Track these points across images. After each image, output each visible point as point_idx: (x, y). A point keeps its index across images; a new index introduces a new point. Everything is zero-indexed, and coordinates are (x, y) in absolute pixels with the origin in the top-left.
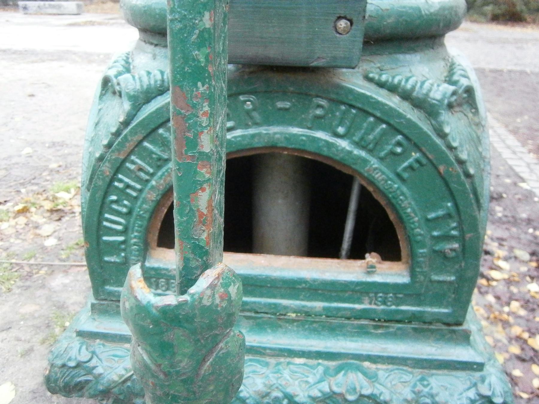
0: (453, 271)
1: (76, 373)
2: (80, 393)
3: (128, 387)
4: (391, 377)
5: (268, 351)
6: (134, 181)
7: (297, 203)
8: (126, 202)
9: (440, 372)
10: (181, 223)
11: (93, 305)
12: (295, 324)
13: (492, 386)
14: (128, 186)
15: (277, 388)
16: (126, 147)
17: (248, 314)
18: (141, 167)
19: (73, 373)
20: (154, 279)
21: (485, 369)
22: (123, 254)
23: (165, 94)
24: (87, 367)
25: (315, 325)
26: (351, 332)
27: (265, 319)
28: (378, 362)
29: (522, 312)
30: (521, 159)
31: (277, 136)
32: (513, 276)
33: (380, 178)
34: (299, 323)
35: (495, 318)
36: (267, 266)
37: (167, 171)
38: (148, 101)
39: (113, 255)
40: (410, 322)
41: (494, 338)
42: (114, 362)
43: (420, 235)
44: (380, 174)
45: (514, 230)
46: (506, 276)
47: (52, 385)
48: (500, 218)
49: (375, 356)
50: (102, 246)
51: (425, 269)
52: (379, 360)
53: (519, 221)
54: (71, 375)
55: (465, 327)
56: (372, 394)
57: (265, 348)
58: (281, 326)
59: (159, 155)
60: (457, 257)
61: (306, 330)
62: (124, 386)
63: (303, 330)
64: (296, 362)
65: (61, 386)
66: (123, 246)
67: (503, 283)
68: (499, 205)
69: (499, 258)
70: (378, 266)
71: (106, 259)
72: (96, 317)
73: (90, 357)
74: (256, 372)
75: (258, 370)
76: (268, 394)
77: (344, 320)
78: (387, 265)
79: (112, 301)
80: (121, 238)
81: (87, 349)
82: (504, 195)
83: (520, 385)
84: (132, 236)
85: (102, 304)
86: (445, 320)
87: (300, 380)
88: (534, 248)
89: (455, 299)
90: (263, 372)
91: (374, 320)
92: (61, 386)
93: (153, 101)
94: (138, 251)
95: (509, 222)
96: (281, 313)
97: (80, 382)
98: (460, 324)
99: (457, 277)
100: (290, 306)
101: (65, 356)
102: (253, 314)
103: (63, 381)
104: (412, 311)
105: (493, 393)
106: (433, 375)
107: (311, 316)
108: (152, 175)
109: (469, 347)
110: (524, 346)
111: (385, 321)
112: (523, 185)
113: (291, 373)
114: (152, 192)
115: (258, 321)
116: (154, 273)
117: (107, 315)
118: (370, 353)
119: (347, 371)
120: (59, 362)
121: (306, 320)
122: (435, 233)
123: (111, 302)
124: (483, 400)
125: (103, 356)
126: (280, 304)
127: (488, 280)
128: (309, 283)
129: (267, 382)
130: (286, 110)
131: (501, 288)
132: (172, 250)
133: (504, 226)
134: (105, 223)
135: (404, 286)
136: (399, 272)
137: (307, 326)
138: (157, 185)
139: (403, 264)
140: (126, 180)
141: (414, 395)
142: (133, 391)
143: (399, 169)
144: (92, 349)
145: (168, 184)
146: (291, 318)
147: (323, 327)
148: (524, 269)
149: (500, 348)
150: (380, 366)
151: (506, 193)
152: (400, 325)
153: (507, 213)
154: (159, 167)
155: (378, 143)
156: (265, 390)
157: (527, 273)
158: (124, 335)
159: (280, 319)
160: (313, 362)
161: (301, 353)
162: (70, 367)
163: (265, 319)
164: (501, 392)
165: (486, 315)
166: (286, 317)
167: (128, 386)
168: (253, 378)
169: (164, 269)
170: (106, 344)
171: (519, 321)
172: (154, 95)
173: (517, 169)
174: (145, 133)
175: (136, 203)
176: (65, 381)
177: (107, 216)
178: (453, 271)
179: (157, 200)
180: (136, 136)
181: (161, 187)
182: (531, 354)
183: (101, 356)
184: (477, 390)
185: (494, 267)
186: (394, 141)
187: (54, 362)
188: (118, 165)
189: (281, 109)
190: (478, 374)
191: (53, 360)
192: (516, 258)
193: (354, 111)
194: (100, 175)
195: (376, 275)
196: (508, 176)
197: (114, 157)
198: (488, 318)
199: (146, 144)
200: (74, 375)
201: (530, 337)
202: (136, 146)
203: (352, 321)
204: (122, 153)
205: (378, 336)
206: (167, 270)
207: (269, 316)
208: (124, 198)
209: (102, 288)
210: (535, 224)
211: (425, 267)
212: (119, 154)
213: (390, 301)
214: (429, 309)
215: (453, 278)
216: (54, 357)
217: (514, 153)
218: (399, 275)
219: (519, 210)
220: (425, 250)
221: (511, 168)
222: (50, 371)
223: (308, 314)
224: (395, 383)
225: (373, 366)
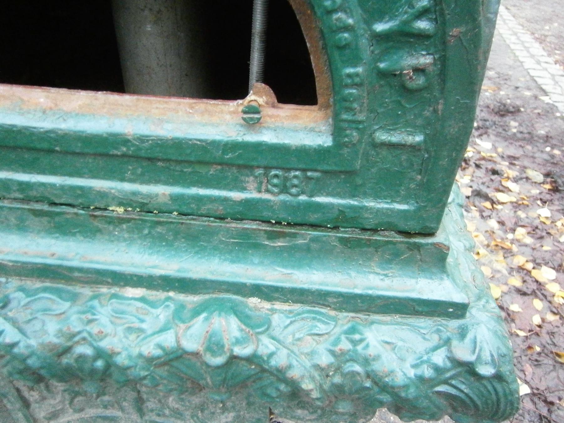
0: (419, 122)
4: (297, 325)
9: (387, 318)
12: (124, 226)
13: (478, 344)
15: (84, 339)
21: (468, 314)
25: (159, 229)
26: (227, 244)
27: (68, 217)
28: (277, 299)
29: (529, 240)
30: (546, 69)
32: (523, 199)
35: (497, 245)
36: (51, 109)
40: (336, 228)
41: (492, 268)
43: (347, 28)
45: (529, 147)
46: (514, 200)
48: (514, 134)
49: (268, 287)
51: (361, 117)
52: (276, 295)
53: (536, 138)
55: (439, 238)
57: (71, 269)
58: (99, 231)
60: (427, 88)
63: (139, 238)
64: (126, 295)
67: (509, 206)
68: (515, 120)
69: (508, 178)
70: (268, 111)
74: (50, 310)
76: (67, 350)
77: (212, 222)
78: (288, 110)
82: (522, 109)
83: (517, 321)
86: (403, 226)
88: (549, 168)
89: (421, 185)
90: (62, 311)
95: (524, 139)
98: (431, 234)
99: (426, 135)
104: (339, 205)
105: (479, 357)
106: (372, 323)
107: (152, 212)
109: (445, 277)
110: (527, 278)
111: (289, 224)
112: (546, 99)
113: (114, 314)
115: (57, 219)
119: (211, 313)
121: (142, 220)
122: (380, 27)
124: (459, 369)
126: (90, 188)
127: (493, 203)
128: (134, 145)
129: (65, 329)
131: (506, 212)
133: (518, 144)
136: (312, 125)
137: (146, 232)
139: (320, 109)
141: (332, 359)
147: (176, 234)
148: (535, 191)
149: (498, 280)
150: (278, 306)
151: (523, 107)
153: (521, 129)
157: (539, 197)
159: (95, 216)
160: (161, 295)
161: (135, 279)
163: (68, 217)
164: (492, 356)
165: (486, 243)
166: (106, 213)
171: (524, 249)
173: (540, 81)
178: (419, 122)
182: (534, 286)
184: (450, 351)
185: (501, 188)
188: (270, 166)
189: (384, 144)
190: (454, 324)
192: (527, 178)
195: (264, 131)
196: (529, 89)
198: (488, 246)
201: (534, 268)
203: (228, 223)
207: (75, 210)
210: (554, 142)
211: (361, 112)
213: (296, 186)
214: (370, 203)
215: (419, 138)
217: (539, 63)
218: (312, 130)
219: (537, 125)
220: (360, 70)
221: (533, 79)
224: (302, 335)
225: (267, 305)
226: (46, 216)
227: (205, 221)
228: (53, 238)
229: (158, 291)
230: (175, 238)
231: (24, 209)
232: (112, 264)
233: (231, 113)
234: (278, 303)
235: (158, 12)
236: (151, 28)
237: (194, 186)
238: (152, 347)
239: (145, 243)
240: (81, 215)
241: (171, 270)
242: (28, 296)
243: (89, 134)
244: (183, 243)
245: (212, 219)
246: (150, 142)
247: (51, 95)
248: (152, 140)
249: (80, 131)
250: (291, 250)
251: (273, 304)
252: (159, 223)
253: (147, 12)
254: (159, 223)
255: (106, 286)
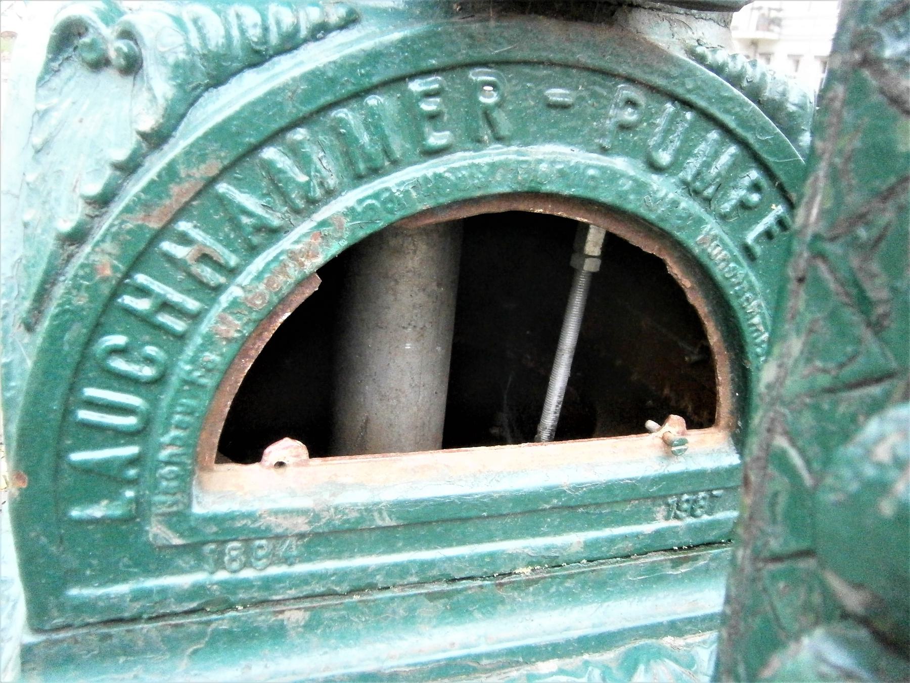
5: (485, 662)
6: (182, 291)
7: (439, 349)
8: (151, 350)
14: (166, 306)
16: (169, 196)
17: (435, 588)
18: (207, 252)
23: (267, 65)
25: (569, 584)
27: (470, 592)
31: (543, 167)
33: (720, 257)
37: (276, 258)
38: (218, 79)
44: (719, 249)
49: (682, 621)
57: (477, 658)
58: (502, 601)
59: (259, 217)
66: (132, 472)
77: (622, 562)
79: (87, 625)
84: (166, 439)
85: (55, 642)
93: (234, 81)
96: (502, 571)
102: (445, 587)
108: (232, 272)
111: (689, 548)
114: (230, 318)
117: (72, 667)
130: (564, 107)
132: (255, 467)
135: (730, 471)
138: (246, 298)
140: (157, 287)
143: (750, 237)
145: (276, 293)
146: (523, 577)
150: (691, 639)
152: (715, 551)
154: (253, 250)
155: (724, 183)
160: (572, 662)
169: (244, 516)
172: (236, 65)
174: (227, 156)
175: (181, 351)
177: (90, 392)
180: (202, 166)
181: (258, 302)
186: (746, 181)
193: (689, 115)
194: (83, 278)
197: (129, 226)
199: (222, 188)
202: (198, 194)
204: (156, 213)
205: (680, 579)
206: (250, 516)
207: (479, 582)
208: (147, 338)
212: (148, 216)
225: (680, 642)
226: (441, 598)
229: (571, 658)
232: (524, 638)
234: (689, 636)
241: (586, 628)
246: (584, 489)
250: (689, 577)
252: (571, 576)
254: (571, 576)
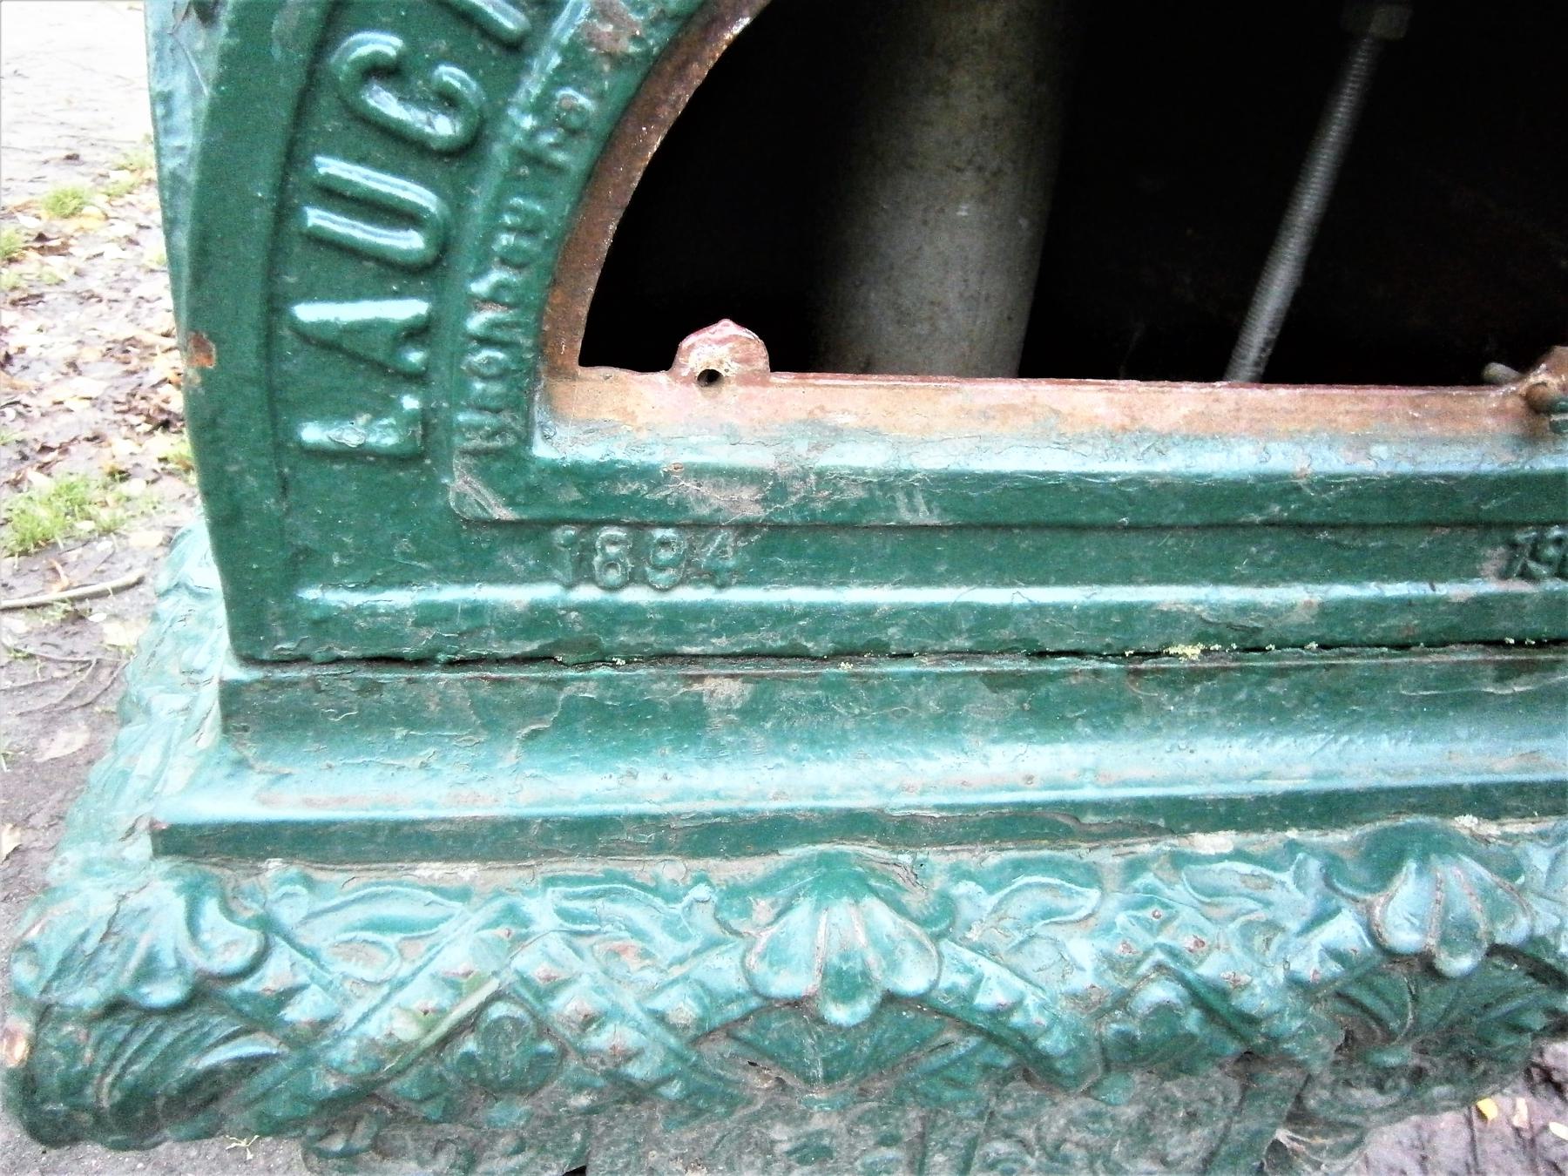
1: (187, 1033)
2: (201, 1122)
3: (469, 1058)
5: (1090, 818)
7: (1024, 222)
8: (450, 75)
10: (573, 295)
11: (231, 695)
15: (1159, 967)
17: (1006, 665)
19: (168, 1038)
20: (571, 532)
22: (410, 403)
24: (246, 997)
26: (1408, 702)
28: (1509, 812)
34: (1213, 684)
39: (349, 416)
42: (384, 956)
47: (49, 1107)
49: (1497, 786)
50: (295, 362)
54: (158, 1047)
56: (1532, 940)
57: (1077, 809)
58: (1135, 707)
61: (1236, 708)
62: (442, 1061)
63: (1222, 713)
65: (105, 1104)
66: (415, 357)
71: (312, 433)
72: (250, 751)
73: (253, 948)
74: (1060, 912)
75: (1064, 904)
76: (1122, 1001)
77: (1390, 656)
79: (338, 660)
80: (407, 309)
81: (229, 913)
84: (480, 287)
85: (281, 685)
87: (1242, 919)
91: (1499, 644)
92: (105, 1104)
94: (503, 375)
97: (212, 1072)
100: (1192, 612)
101: (107, 957)
102: (1025, 666)
103: (113, 1085)
111: (1540, 645)
113: (1207, 900)
116: (575, 495)
118: (1487, 778)
120: (88, 996)
123: (333, 670)
125: (319, 936)
126: (1150, 606)
129: (1118, 950)
132: (661, 377)
134: (317, 218)
142: (490, 1075)
144: (255, 909)
146: (1183, 663)
150: (1513, 827)
156: (1114, 981)
158: (414, 823)
159: (1138, 673)
162: (151, 1012)
166: (1163, 663)
167: (467, 1054)
168: (1055, 942)
170: (319, 875)
175: (514, 85)
176: (128, 1078)
179: (647, 54)
183: (306, 938)
187: (54, 996)
191: (45, 990)
200: (171, 1045)
207: (1093, 664)
208: (443, 45)
209: (281, 599)
216: (49, 973)
222: (34, 1044)
223: (1252, 644)
227: (1376, 656)
228: (1018, 739)
230: (1302, 703)
231: (975, 673)
233: (1495, 413)
235: (994, 174)
236: (968, 210)
237: (1371, 579)
238: (1316, 959)
239: (1232, 724)
240: (1109, 672)
242: (991, 890)
243: (1216, 480)
244: (1316, 711)
245: (1385, 649)
247: (1117, 397)
248: (1346, 484)
249: (1199, 476)
251: (1503, 825)
253: (969, 174)
255: (1145, 839)
